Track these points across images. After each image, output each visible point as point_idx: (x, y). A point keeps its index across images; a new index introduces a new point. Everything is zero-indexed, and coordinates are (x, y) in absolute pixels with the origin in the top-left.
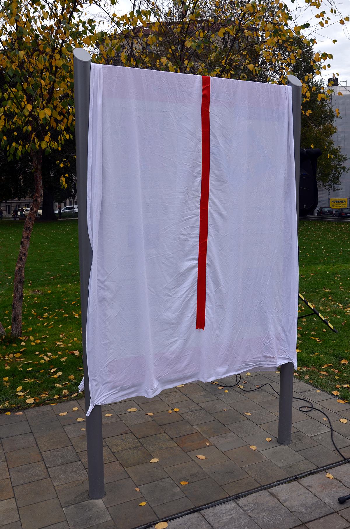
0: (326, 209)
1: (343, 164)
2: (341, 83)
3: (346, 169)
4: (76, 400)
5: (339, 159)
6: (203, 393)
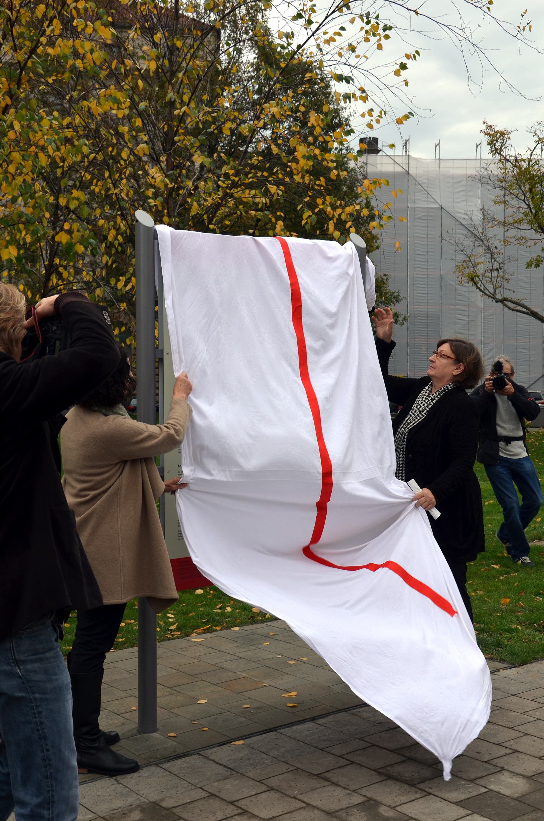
2: (384, 149)
6: (236, 644)
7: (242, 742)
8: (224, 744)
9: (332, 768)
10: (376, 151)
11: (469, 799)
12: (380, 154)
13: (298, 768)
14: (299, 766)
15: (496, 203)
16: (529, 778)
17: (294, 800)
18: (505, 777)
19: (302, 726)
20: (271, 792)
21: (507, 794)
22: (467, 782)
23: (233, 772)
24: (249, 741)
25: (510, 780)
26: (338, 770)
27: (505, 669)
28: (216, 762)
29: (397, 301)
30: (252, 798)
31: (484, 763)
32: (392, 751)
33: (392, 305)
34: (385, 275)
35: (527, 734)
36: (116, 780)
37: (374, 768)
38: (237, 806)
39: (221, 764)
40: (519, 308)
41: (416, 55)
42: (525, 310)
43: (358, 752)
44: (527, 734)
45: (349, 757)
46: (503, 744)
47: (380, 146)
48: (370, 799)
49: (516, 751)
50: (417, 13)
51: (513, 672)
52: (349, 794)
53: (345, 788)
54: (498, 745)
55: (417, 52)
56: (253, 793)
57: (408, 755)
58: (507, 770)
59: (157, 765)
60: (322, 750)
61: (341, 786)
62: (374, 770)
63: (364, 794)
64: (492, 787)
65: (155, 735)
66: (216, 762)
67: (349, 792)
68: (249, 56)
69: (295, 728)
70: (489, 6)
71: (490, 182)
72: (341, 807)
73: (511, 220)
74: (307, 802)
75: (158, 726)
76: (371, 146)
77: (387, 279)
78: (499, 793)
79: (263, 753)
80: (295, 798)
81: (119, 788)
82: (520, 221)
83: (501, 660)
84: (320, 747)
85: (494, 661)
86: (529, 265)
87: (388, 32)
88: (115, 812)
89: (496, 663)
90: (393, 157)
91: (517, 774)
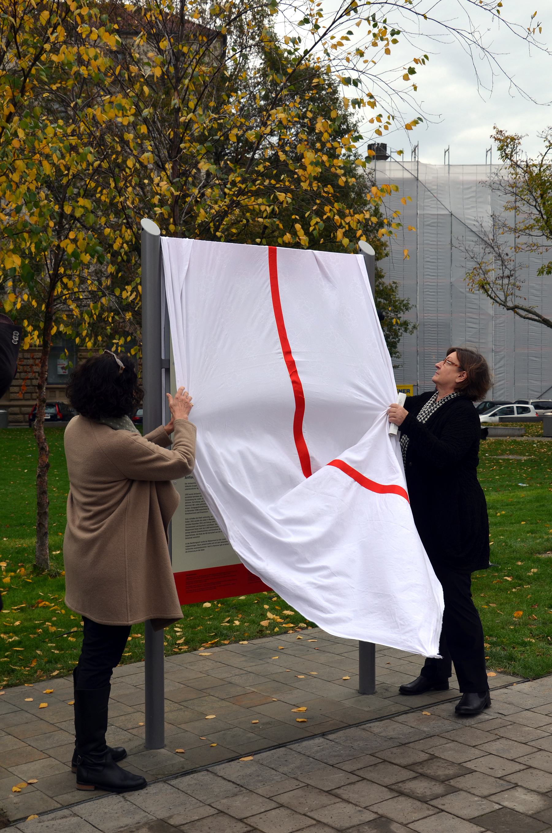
1: (404, 316)
4: (62, 677)
5: (395, 306)
7: (250, 758)
8: (232, 760)
9: (343, 784)
10: (385, 157)
11: (482, 815)
12: (389, 160)
13: (308, 785)
14: (309, 782)
15: (507, 209)
16: (544, 794)
17: (304, 817)
18: (519, 794)
19: (311, 742)
20: (281, 808)
21: (521, 811)
22: (480, 799)
23: (242, 789)
24: (258, 757)
25: (524, 797)
26: (348, 786)
27: (518, 683)
28: (224, 779)
29: (407, 309)
30: (262, 815)
31: (498, 780)
32: (405, 767)
33: (402, 313)
34: (394, 283)
35: (541, 750)
36: (123, 797)
37: (385, 785)
38: (246, 824)
39: (229, 781)
40: (530, 316)
41: (425, 60)
42: (537, 318)
43: (369, 768)
44: (541, 750)
45: (361, 773)
46: (516, 760)
47: (388, 152)
48: (382, 816)
49: (530, 767)
50: (426, 18)
51: (526, 686)
52: (360, 811)
53: (356, 805)
54: (512, 760)
55: (426, 57)
56: (263, 810)
57: (420, 771)
58: (521, 786)
59: (165, 782)
60: (332, 766)
61: (352, 803)
62: (386, 787)
63: (375, 811)
64: (506, 804)
65: (162, 750)
66: (224, 779)
67: (360, 809)
68: (256, 62)
69: (305, 743)
70: (498, 8)
71: (500, 188)
72: (351, 824)
73: (522, 226)
74: (317, 818)
75: (166, 742)
76: (379, 152)
77: (396, 287)
78: (513, 810)
79: (273, 769)
80: (305, 815)
81: (127, 805)
82: (531, 228)
83: (514, 674)
84: (331, 763)
85: (507, 675)
86: (541, 272)
87: (396, 37)
88: (122, 829)
89: (509, 677)
90: (401, 164)
91: (532, 790)
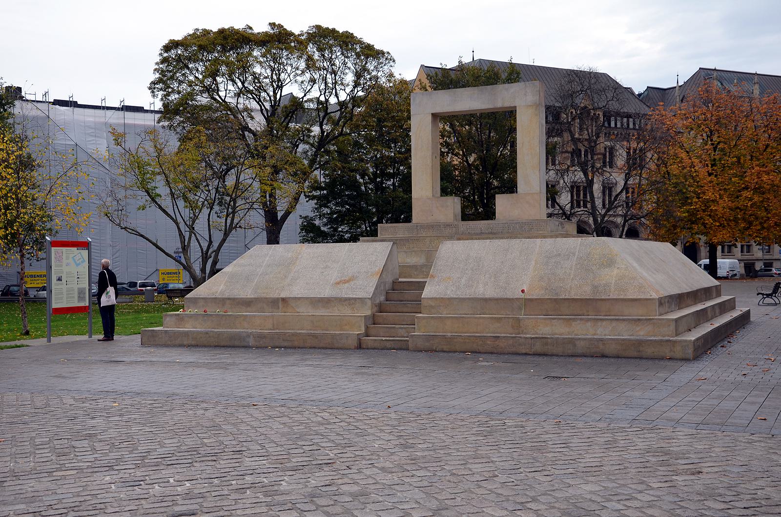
0: (16, 288)
3: (54, 232)
40: (134, 232)
86: (139, 209)
